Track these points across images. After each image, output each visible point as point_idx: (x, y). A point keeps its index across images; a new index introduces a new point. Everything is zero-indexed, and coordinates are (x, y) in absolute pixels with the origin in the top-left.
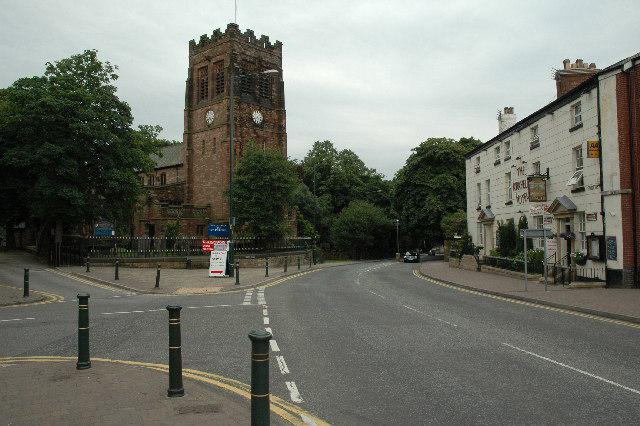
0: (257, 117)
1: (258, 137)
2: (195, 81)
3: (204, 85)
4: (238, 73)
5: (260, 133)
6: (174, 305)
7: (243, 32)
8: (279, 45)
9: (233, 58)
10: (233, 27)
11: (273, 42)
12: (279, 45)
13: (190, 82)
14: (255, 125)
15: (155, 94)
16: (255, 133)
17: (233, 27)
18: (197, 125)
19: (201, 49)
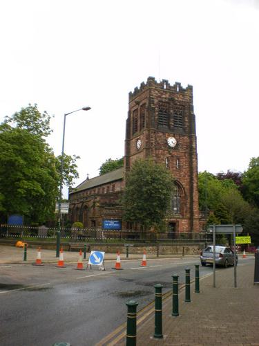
0: (172, 141)
1: (172, 156)
2: (132, 119)
3: (135, 121)
4: (162, 113)
5: (175, 153)
6: (188, 268)
7: (158, 82)
8: (190, 88)
9: (38, 211)
10: (151, 80)
11: (184, 86)
12: (190, 88)
13: (128, 121)
14: (170, 147)
15: (90, 143)
16: (170, 154)
17: (151, 80)
18: (133, 151)
19: (136, 97)
